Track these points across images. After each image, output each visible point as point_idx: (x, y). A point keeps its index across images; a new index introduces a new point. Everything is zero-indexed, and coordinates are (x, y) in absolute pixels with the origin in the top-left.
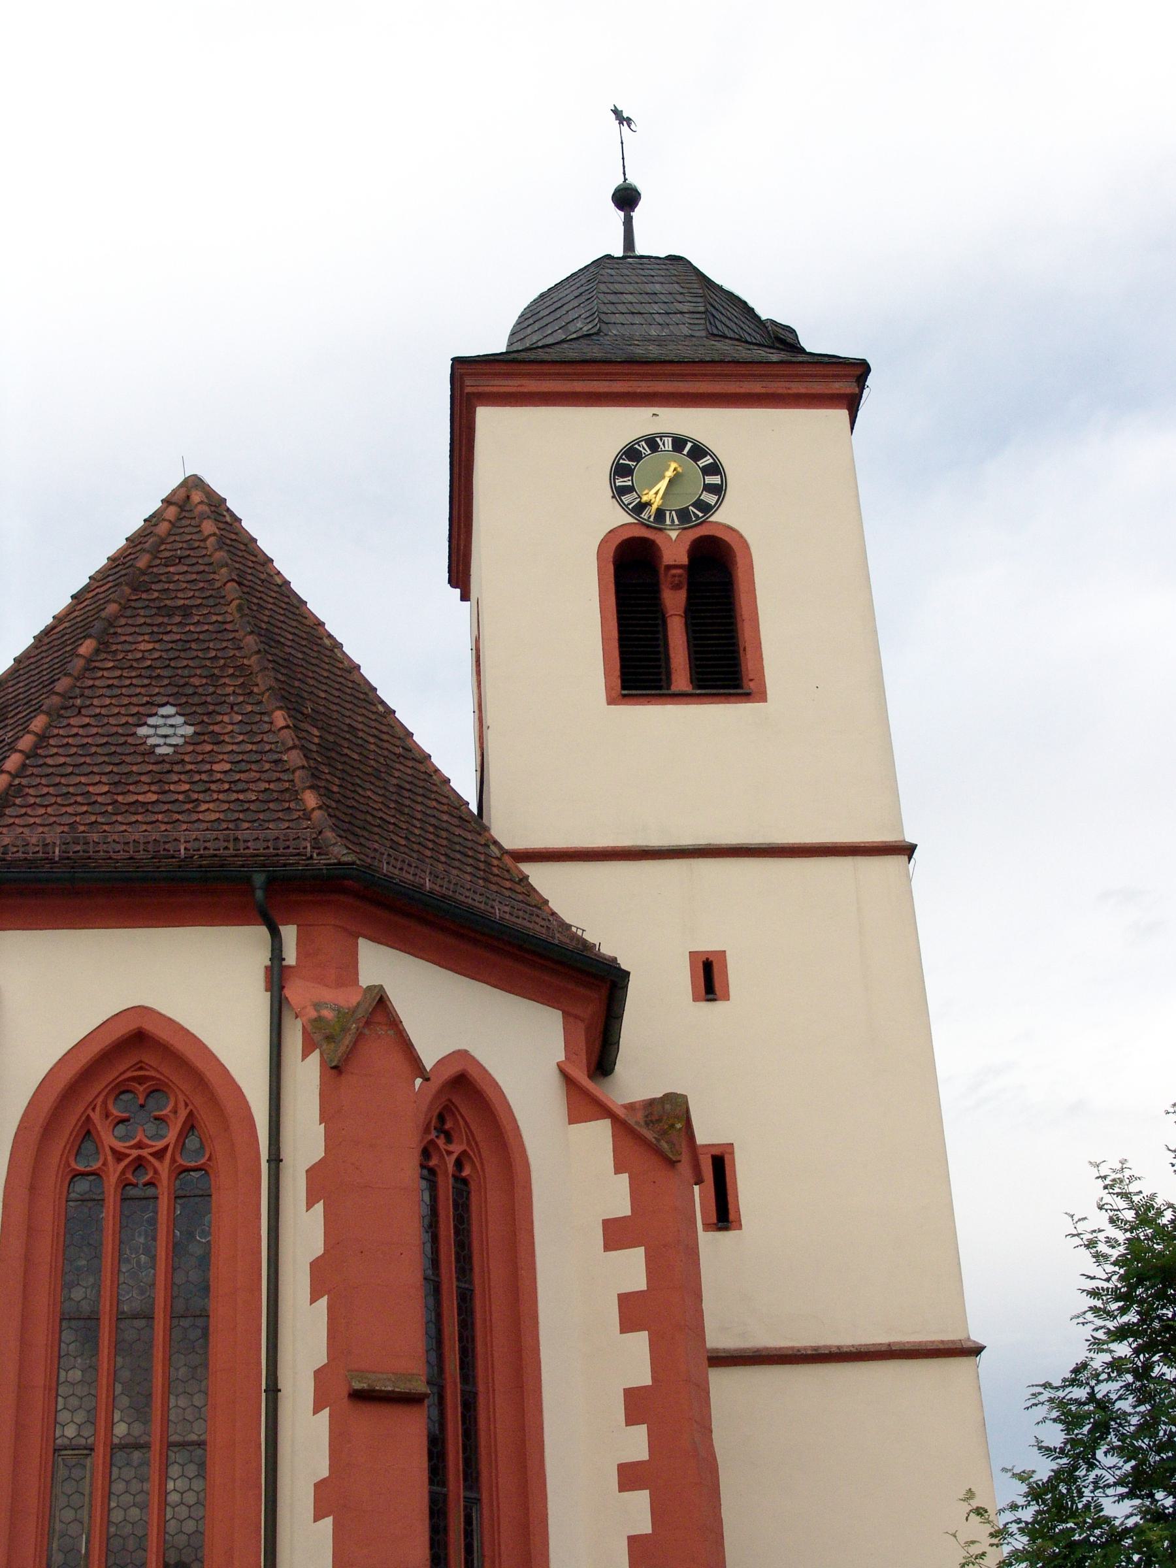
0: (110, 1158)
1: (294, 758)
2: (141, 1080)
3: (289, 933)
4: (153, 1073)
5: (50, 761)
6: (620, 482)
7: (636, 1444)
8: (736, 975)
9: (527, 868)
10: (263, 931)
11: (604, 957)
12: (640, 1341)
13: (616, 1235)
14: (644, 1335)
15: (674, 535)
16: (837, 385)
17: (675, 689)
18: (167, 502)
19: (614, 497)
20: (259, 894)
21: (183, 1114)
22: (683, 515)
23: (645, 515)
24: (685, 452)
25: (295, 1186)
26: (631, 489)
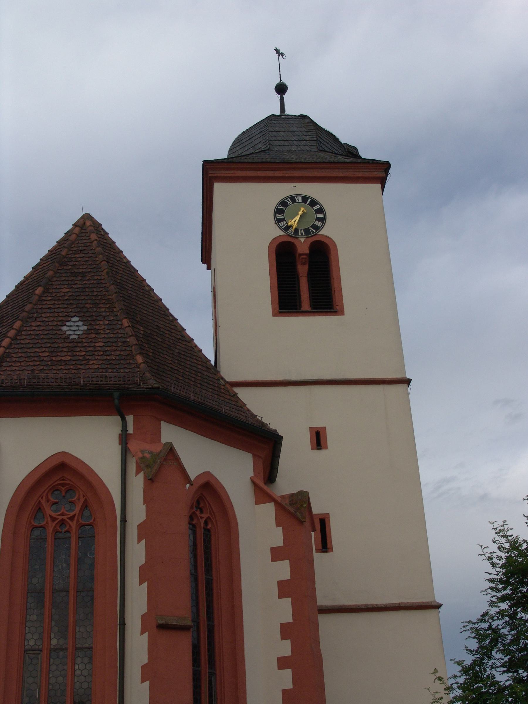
0: (49, 520)
1: (132, 340)
2: (63, 485)
3: (130, 419)
4: (68, 482)
5: (22, 342)
6: (278, 216)
7: (285, 648)
8: (331, 438)
9: (236, 390)
10: (118, 418)
11: (271, 430)
12: (287, 602)
13: (277, 554)
14: (289, 599)
15: (302, 240)
16: (376, 173)
17: (303, 309)
18: (75, 225)
19: (275, 223)
20: (116, 401)
21: (82, 500)
22: (307, 231)
23: (289, 231)
24: (308, 203)
25: (132, 533)
26: (283, 220)
